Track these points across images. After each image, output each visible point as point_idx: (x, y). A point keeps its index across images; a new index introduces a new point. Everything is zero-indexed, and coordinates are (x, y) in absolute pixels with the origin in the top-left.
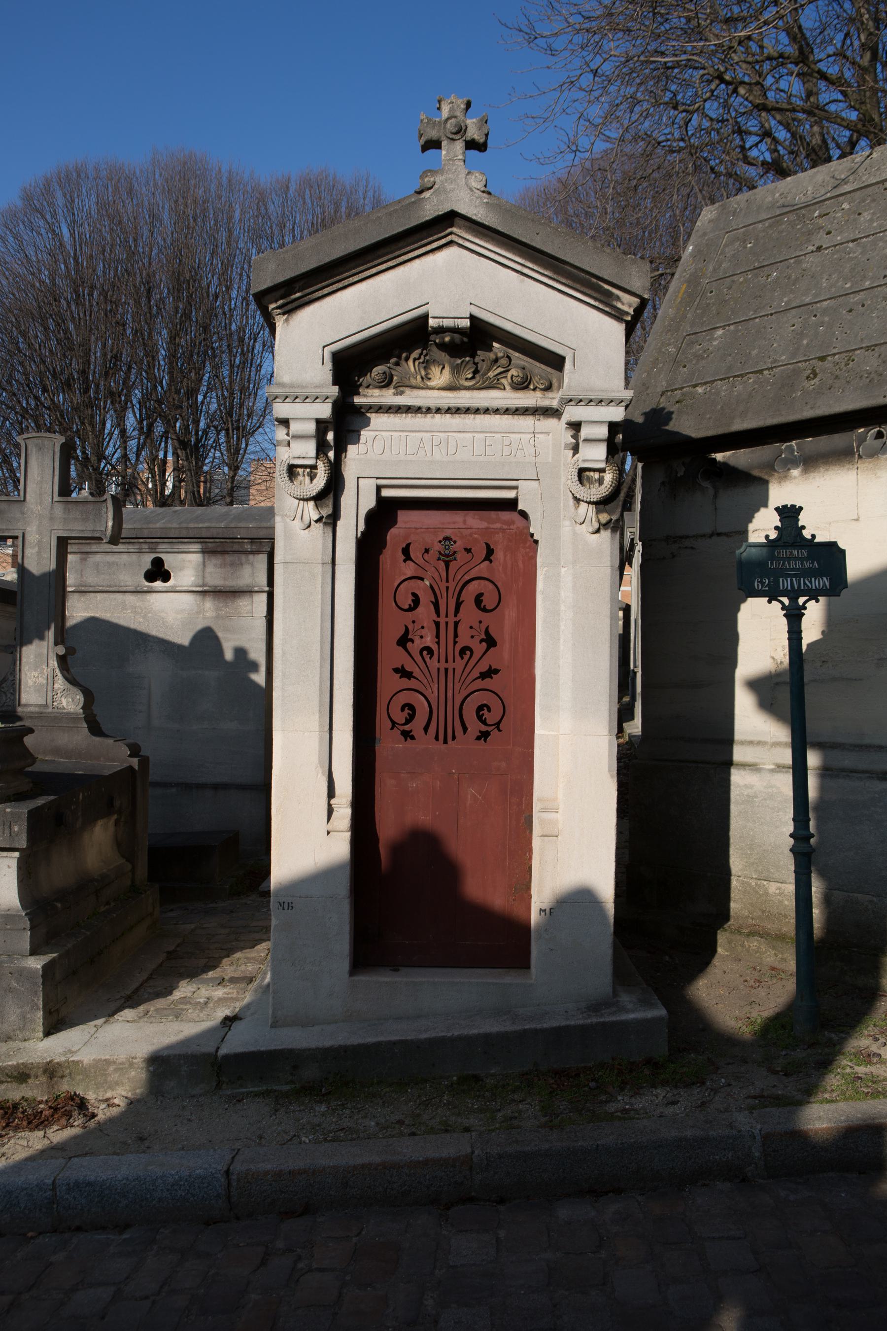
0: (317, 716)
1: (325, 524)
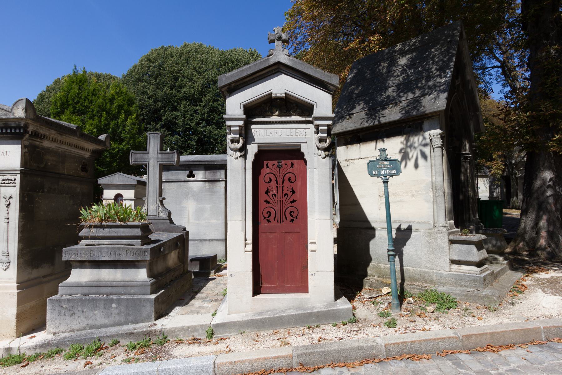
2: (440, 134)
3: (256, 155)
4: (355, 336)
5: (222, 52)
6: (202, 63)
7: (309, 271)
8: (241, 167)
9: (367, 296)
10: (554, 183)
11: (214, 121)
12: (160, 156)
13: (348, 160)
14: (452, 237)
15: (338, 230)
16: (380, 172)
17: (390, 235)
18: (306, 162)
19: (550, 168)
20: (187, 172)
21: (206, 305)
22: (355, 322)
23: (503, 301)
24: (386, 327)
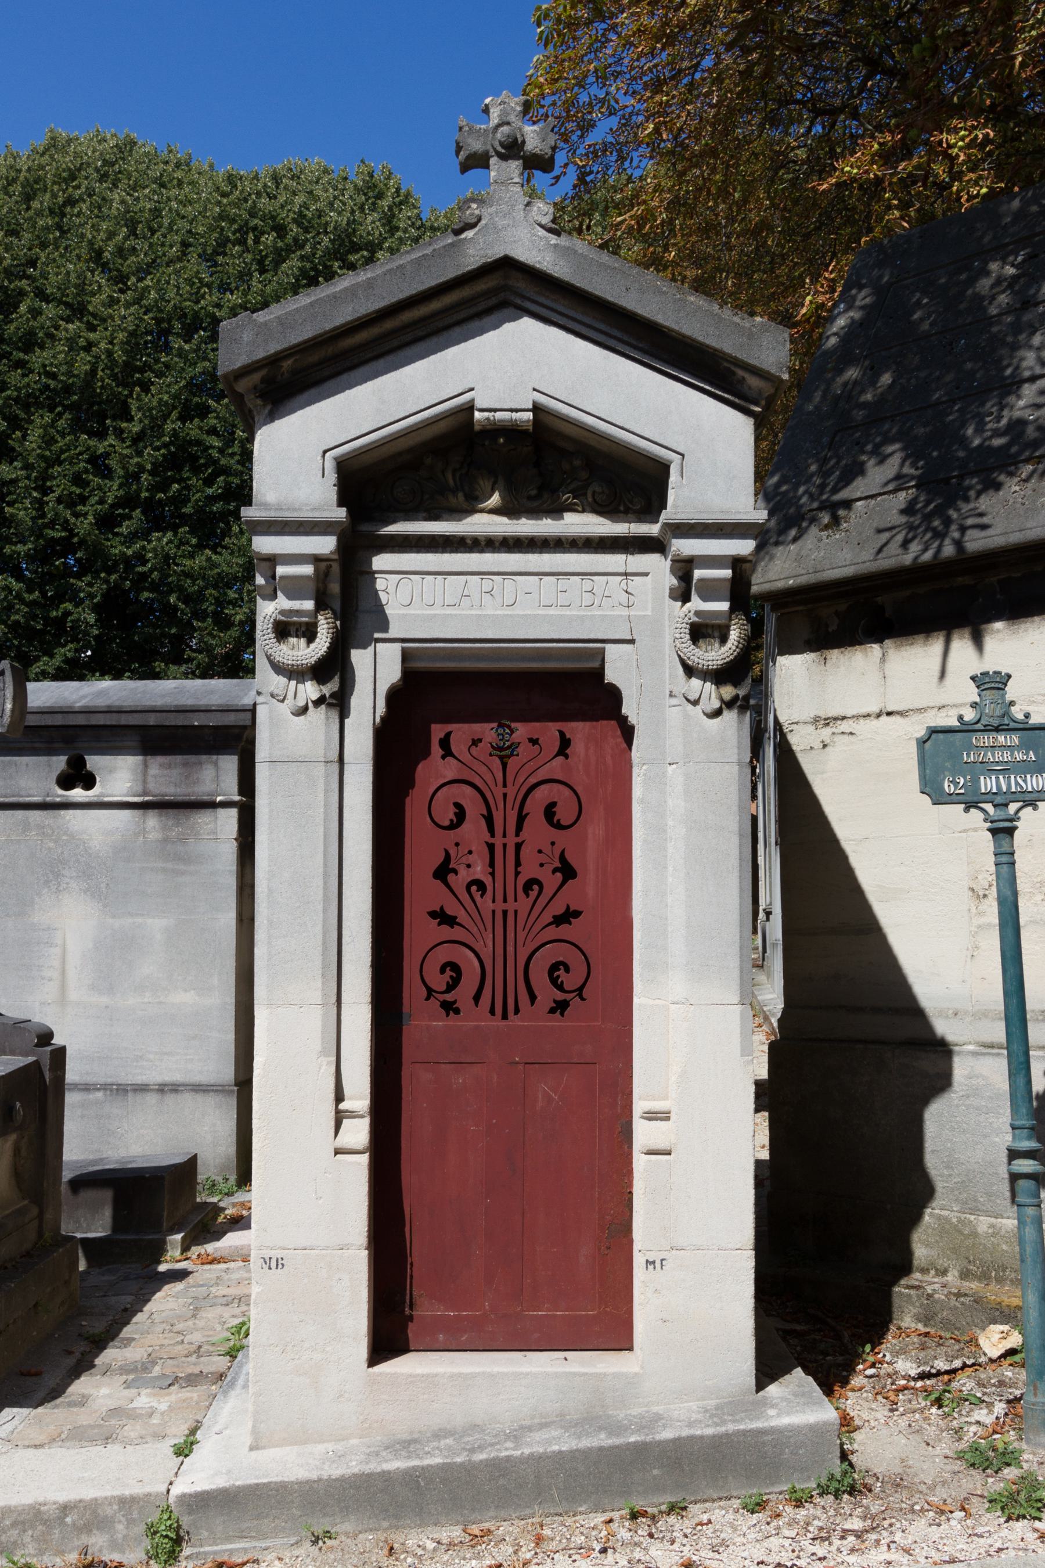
3: (394, 696)
4: (852, 1559)
5: (231, 179)
6: (133, 233)
7: (637, 1246)
8: (320, 753)
9: (907, 1366)
11: (188, 510)
13: (828, 721)
15: (774, 1049)
16: (976, 781)
17: (1021, 1081)
18: (628, 732)
20: (60, 763)
21: (144, 1400)
22: (852, 1491)
24: (996, 1518)
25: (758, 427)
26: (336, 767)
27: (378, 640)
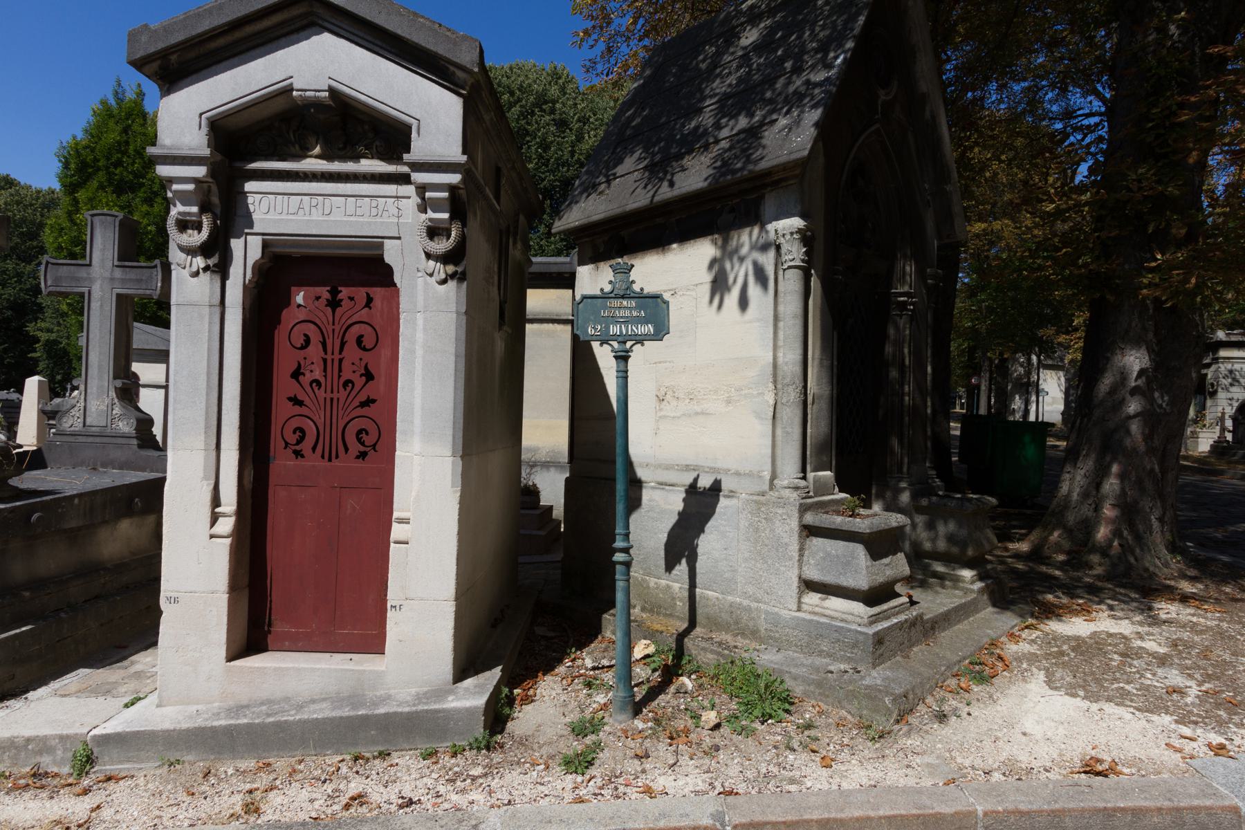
0: (202, 437)
1: (213, 272)
2: (799, 231)
3: (258, 267)
10: (1148, 383)
12: (118, 273)
14: (810, 518)
19: (1137, 343)
23: (921, 707)
24: (558, 770)
25: (465, 103)
26: (217, 311)
27: (247, 234)
